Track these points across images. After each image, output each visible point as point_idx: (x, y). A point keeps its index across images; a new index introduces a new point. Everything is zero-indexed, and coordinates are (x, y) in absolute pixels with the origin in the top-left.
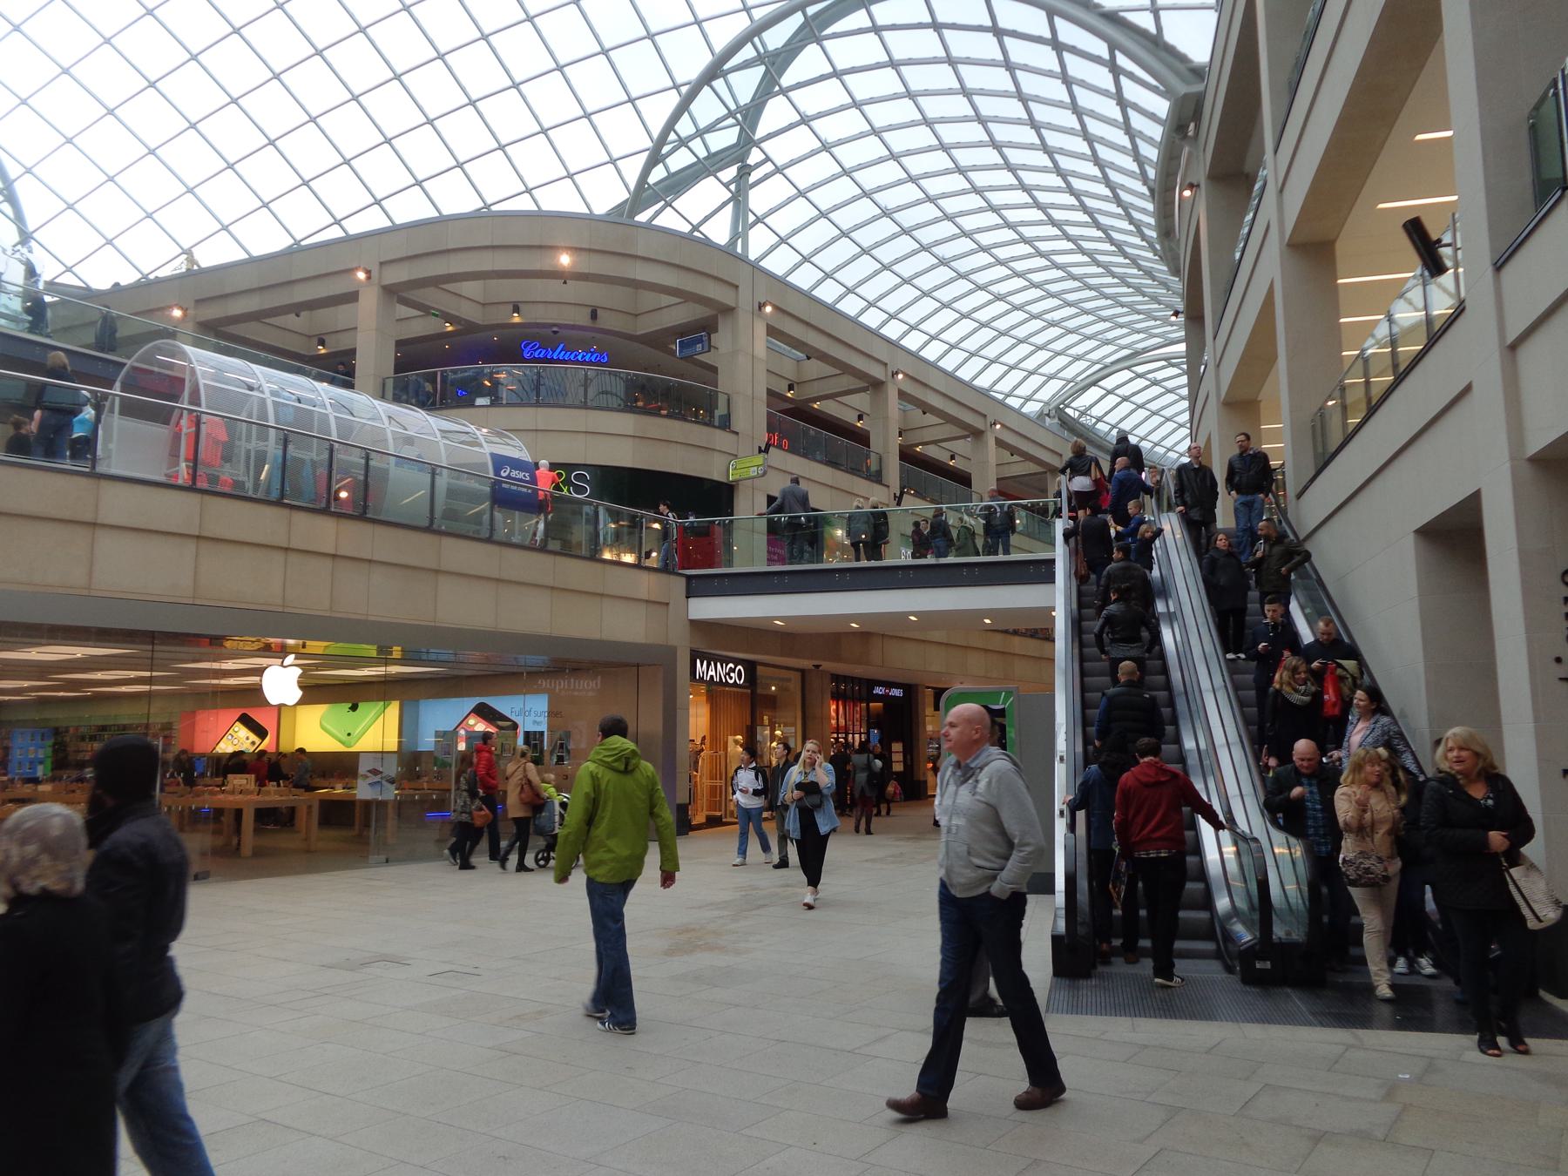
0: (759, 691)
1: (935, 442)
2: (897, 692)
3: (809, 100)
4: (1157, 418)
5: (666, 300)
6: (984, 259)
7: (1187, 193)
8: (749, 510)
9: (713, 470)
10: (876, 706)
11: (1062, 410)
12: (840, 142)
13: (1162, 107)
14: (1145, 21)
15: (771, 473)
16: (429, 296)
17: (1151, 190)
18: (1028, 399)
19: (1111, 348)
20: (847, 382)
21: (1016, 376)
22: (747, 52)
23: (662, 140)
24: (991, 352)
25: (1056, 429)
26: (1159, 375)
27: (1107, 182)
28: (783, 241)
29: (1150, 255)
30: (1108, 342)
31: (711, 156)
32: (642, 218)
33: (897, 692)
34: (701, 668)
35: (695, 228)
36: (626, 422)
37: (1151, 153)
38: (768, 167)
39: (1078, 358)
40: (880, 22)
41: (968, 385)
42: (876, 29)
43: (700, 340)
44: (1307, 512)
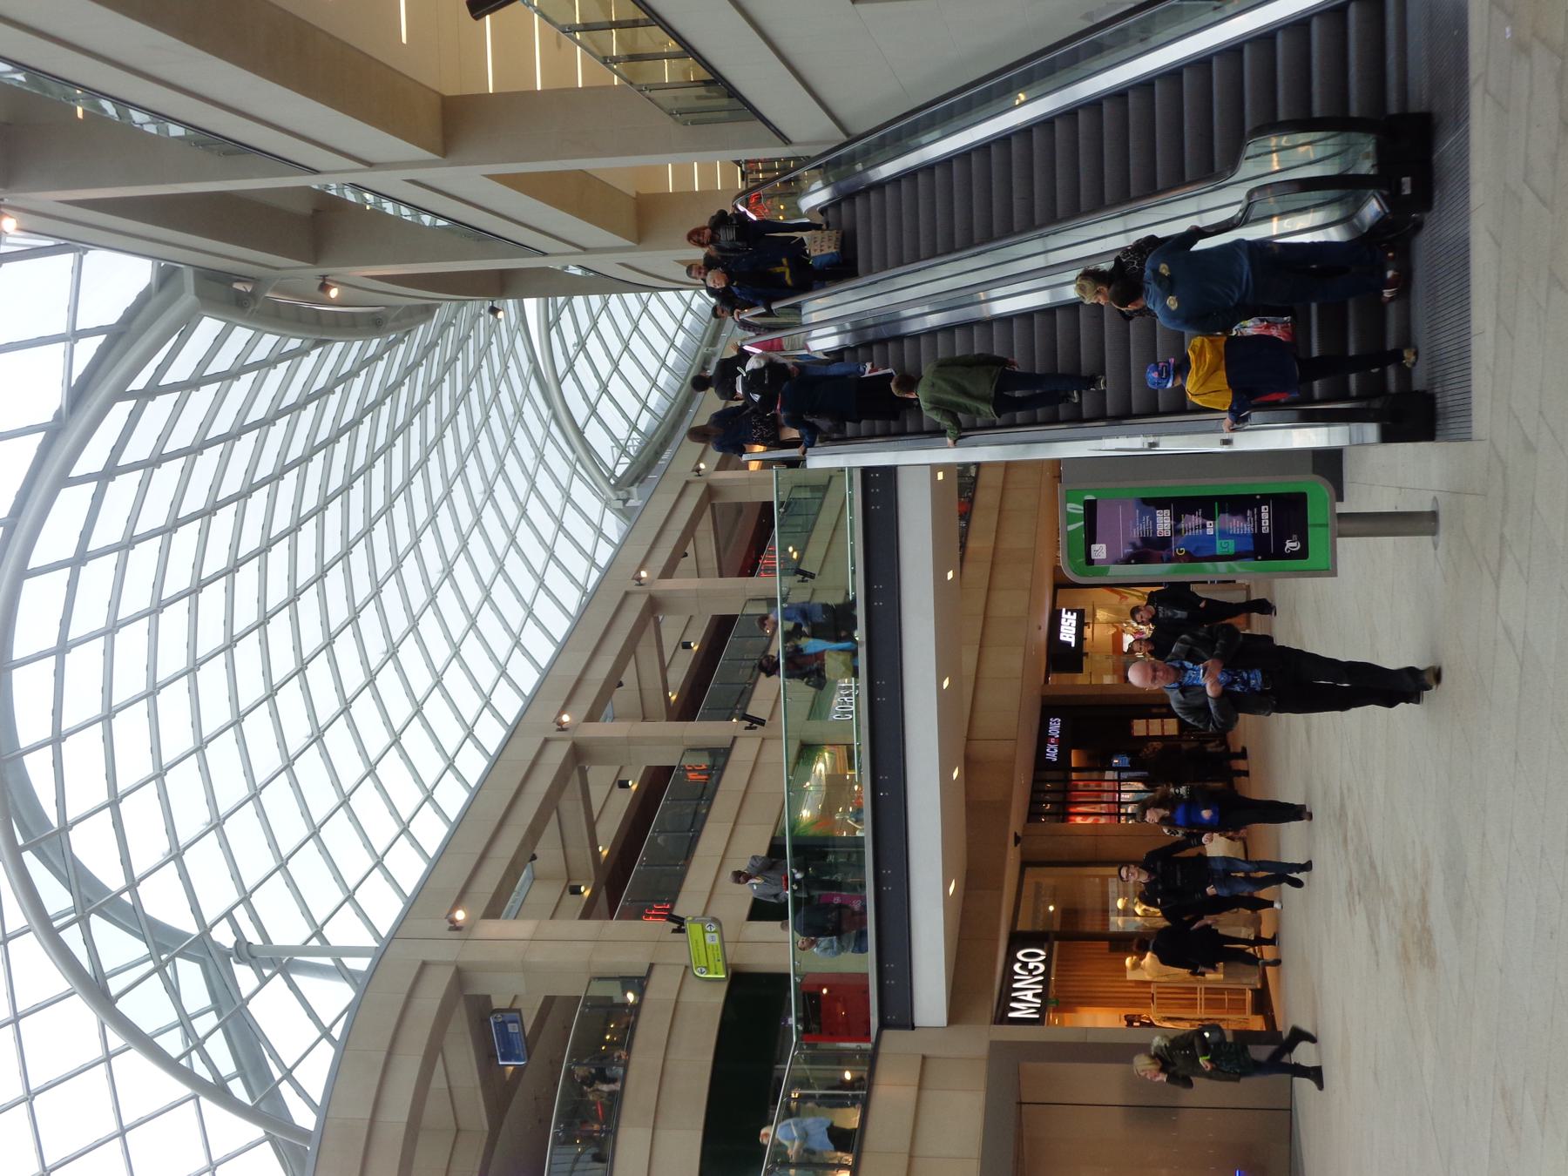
0: (1057, 927)
1: (664, 670)
2: (1055, 727)
3: (148, 846)
4: (641, 342)
5: (438, 1081)
6: (369, 618)
7: (334, 293)
8: (778, 948)
10: (1075, 759)
11: (619, 480)
12: (212, 801)
13: (209, 327)
14: (87, 350)
15: (715, 911)
17: (317, 344)
18: (600, 533)
19: (527, 408)
20: (570, 803)
21: (564, 549)
22: (72, 938)
23: (187, 1076)
24: (527, 585)
25: (647, 489)
26: (571, 339)
27: (267, 422)
28: (350, 897)
30: (519, 413)
31: (217, 1007)
33: (1055, 727)
34: (1021, 1011)
35: (326, 1033)
36: (631, 1143)
37: (269, 341)
38: (241, 914)
39: (540, 457)
40: (46, 732)
41: (578, 622)
42: (57, 739)
43: (502, 1026)
44: (808, 128)
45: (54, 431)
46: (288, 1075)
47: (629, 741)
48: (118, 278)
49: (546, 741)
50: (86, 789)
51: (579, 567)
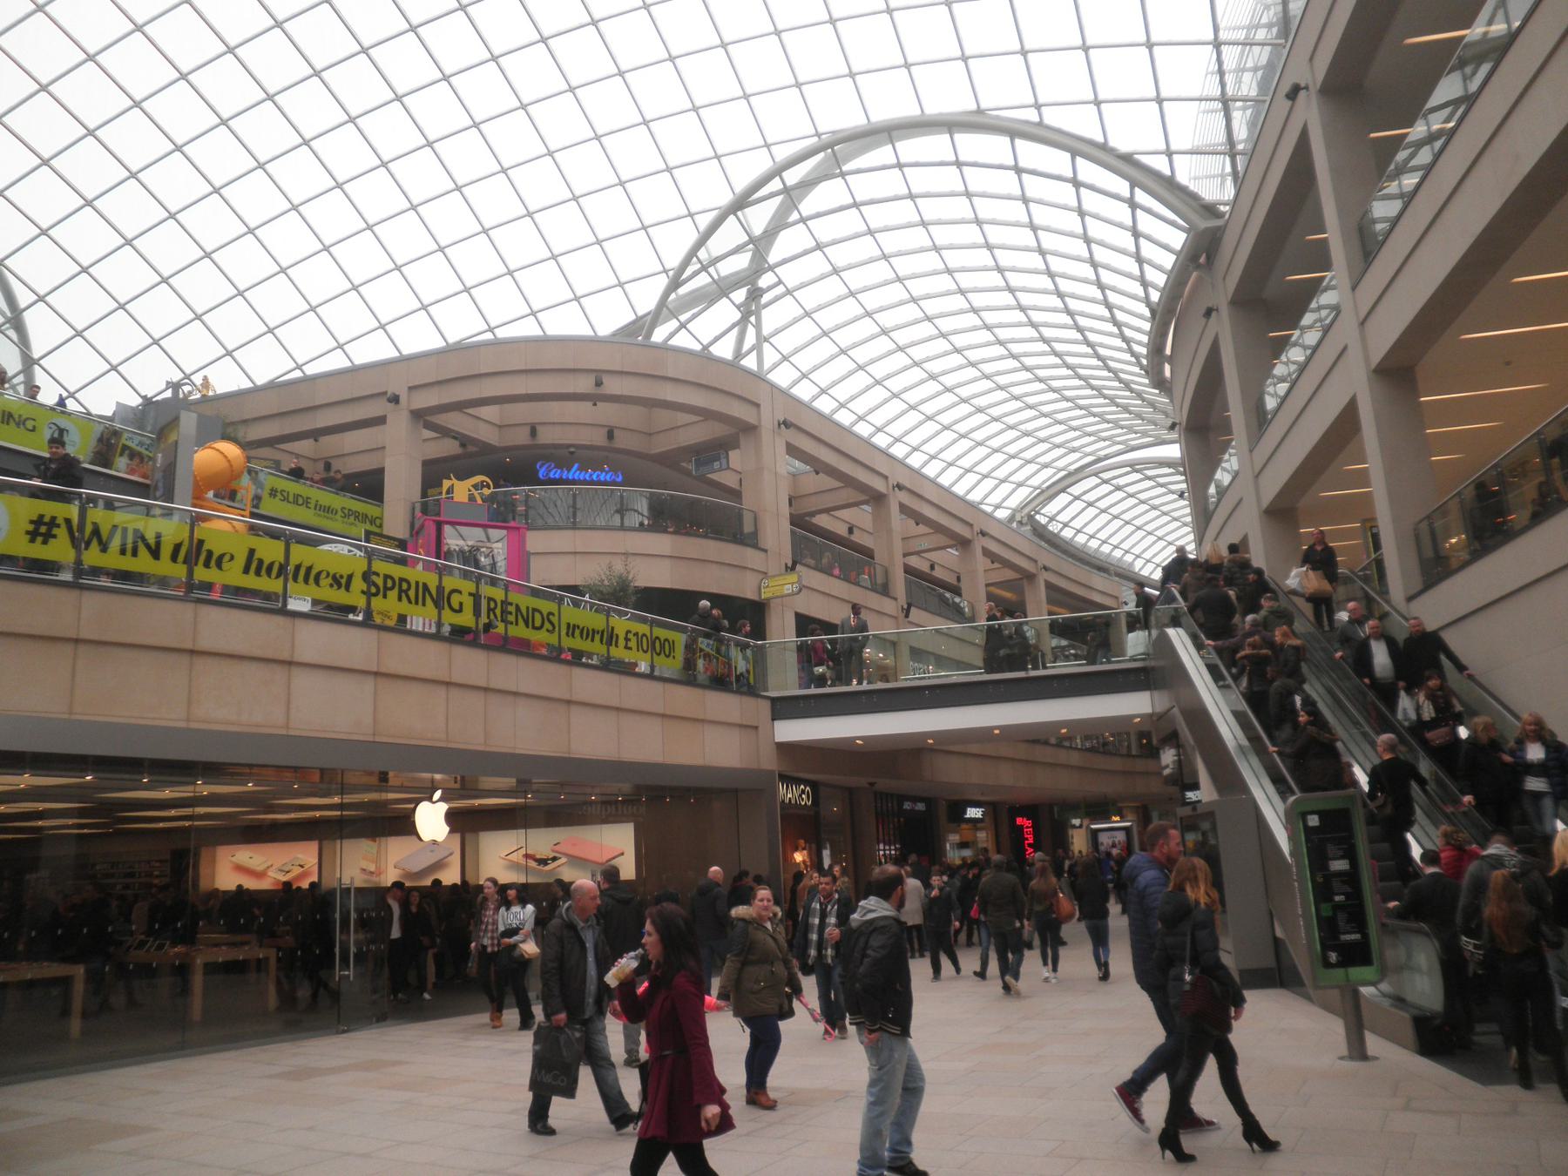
1: (918, 553)
2: (921, 806)
3: (825, 229)
9: (745, 588)
13: (1178, 239)
14: (1160, 164)
16: (454, 421)
17: (1153, 312)
19: (1077, 455)
20: (849, 495)
22: (775, 185)
25: (1029, 535)
29: (1137, 370)
30: (1074, 450)
32: (659, 336)
33: (921, 806)
35: (706, 348)
36: (662, 543)
38: (780, 290)
39: (1046, 466)
45: (1104, 147)
46: (683, 326)
47: (890, 531)
48: (1212, 181)
49: (886, 478)
50: (864, 187)
51: (995, 499)
